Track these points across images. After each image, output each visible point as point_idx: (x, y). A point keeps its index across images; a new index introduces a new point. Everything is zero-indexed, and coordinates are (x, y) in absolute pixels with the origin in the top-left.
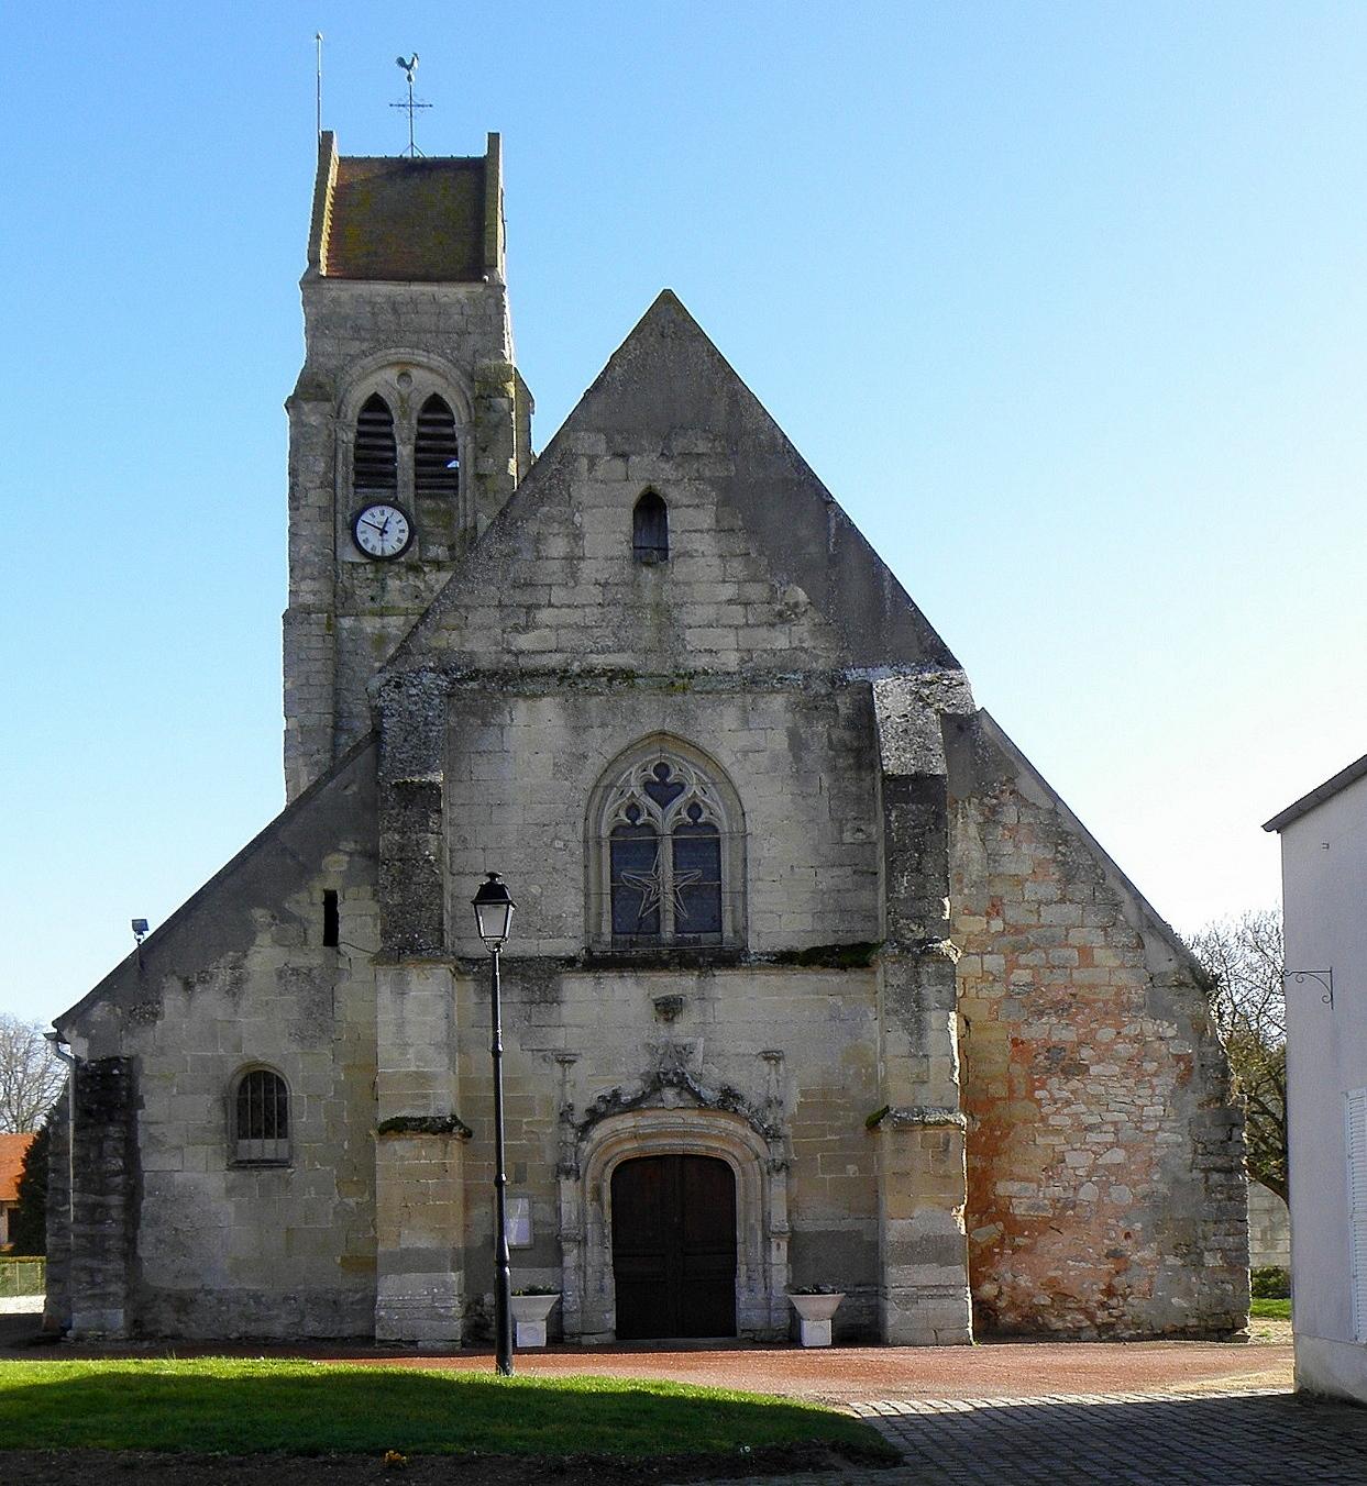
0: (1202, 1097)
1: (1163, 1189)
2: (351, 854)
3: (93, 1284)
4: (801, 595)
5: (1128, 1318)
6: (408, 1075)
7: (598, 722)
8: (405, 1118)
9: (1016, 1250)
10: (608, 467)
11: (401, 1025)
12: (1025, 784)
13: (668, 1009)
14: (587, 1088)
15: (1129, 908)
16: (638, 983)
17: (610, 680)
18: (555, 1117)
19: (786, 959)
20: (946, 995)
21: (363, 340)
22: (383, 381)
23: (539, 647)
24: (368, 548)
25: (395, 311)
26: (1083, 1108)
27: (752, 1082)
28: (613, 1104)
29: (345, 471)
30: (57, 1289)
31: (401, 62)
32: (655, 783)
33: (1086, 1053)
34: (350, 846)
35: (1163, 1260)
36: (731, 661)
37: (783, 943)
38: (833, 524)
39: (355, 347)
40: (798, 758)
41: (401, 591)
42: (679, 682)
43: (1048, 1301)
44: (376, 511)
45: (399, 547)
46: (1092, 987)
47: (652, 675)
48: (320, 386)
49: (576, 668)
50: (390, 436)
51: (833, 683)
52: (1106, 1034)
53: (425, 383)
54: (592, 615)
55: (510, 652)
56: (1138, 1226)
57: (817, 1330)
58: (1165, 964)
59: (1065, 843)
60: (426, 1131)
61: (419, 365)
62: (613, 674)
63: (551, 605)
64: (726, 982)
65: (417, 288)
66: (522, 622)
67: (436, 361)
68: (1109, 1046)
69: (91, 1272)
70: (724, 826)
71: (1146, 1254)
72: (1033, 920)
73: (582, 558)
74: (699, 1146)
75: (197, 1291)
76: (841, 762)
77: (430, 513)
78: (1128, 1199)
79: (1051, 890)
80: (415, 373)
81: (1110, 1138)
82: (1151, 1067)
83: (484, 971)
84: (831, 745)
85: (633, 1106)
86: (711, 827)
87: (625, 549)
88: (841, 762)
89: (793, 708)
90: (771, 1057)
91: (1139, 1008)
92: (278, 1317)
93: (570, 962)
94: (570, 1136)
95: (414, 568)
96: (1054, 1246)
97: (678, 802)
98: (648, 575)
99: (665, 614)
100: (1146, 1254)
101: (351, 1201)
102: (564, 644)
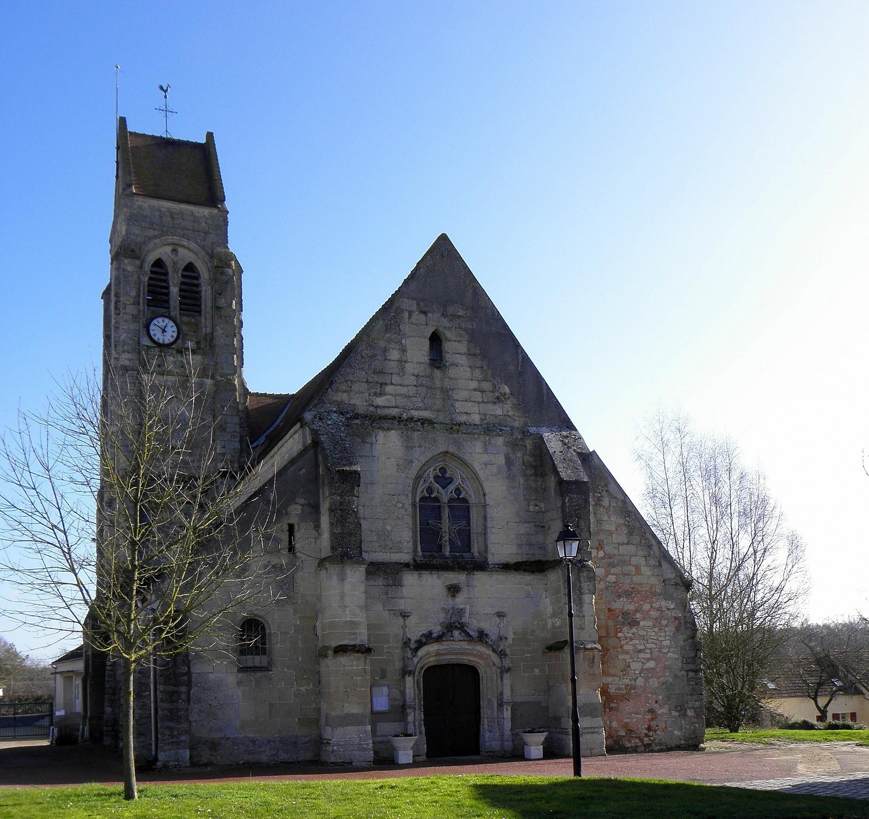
0: (685, 637)
1: (670, 680)
2: (303, 506)
3: (172, 736)
4: (507, 390)
5: (657, 741)
6: (346, 622)
7: (417, 445)
8: (345, 645)
9: (611, 709)
10: (417, 317)
11: (342, 596)
12: (612, 487)
13: (454, 590)
14: (415, 630)
15: (655, 548)
16: (439, 578)
17: (422, 424)
18: (400, 644)
19: (506, 567)
20: (591, 587)
21: (155, 229)
22: (163, 252)
23: (387, 405)
24: (156, 338)
25: (172, 216)
26: (637, 642)
27: (489, 626)
28: (428, 638)
29: (145, 297)
30: (143, 739)
31: (161, 88)
32: (439, 477)
33: (638, 615)
34: (302, 501)
35: (671, 713)
36: (476, 419)
37: (504, 559)
38: (520, 357)
39: (151, 233)
40: (509, 469)
41: (174, 363)
42: (455, 427)
43: (624, 734)
44: (160, 319)
45: (172, 340)
46: (641, 584)
47: (441, 423)
48: (133, 251)
49: (405, 416)
50: (166, 281)
51: (524, 433)
52: (647, 607)
53: (186, 256)
54: (412, 391)
55: (373, 406)
56: (661, 697)
57: (536, 750)
58: (670, 575)
59: (629, 516)
60: (358, 652)
61: (183, 246)
62: (424, 421)
63: (392, 384)
64: (480, 577)
65: (184, 206)
66: (378, 391)
67: (192, 245)
68: (648, 612)
69: (171, 729)
70: (473, 500)
71: (664, 710)
72: (616, 552)
73: (406, 362)
74: (465, 659)
75: (221, 738)
76: (528, 472)
77: (187, 324)
78: (657, 685)
79: (623, 538)
80: (180, 250)
81: (648, 656)
82: (664, 622)
83: (375, 569)
84: (524, 464)
85: (439, 639)
86: (465, 500)
87: (426, 359)
88: (528, 472)
89: (507, 444)
90: (500, 615)
91: (660, 595)
92: (265, 751)
93: (407, 565)
94: (409, 654)
95: (180, 352)
96: (627, 707)
97: (452, 487)
98: (437, 373)
99: (446, 393)
100: (664, 710)
101: (303, 689)
102: (399, 404)
